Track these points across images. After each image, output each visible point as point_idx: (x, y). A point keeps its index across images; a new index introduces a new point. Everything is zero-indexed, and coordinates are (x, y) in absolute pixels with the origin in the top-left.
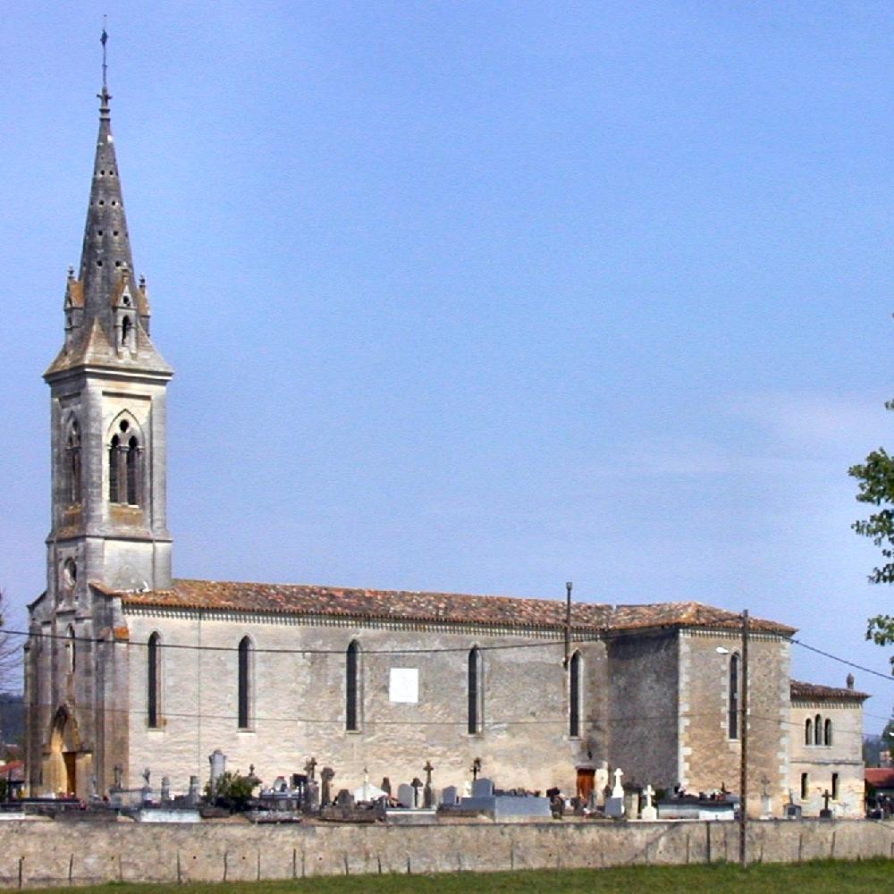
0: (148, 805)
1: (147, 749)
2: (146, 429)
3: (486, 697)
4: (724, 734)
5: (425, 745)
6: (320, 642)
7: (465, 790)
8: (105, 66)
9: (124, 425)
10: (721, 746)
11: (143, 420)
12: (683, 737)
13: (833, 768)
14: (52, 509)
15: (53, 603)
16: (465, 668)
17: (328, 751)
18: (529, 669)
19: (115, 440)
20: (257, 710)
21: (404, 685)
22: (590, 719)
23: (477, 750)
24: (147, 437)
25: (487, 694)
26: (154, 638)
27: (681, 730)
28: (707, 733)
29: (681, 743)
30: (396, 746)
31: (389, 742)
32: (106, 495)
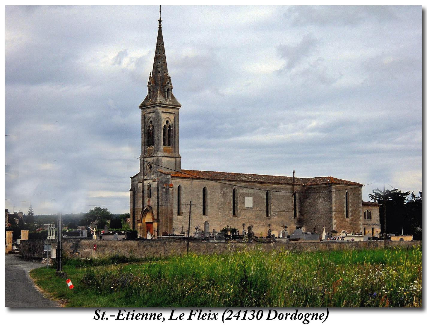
0: (212, 238)
1: (177, 221)
2: (173, 123)
3: (271, 205)
4: (345, 216)
5: (255, 220)
6: (225, 189)
7: (265, 235)
8: (160, 11)
9: (167, 122)
10: (344, 220)
11: (173, 121)
12: (334, 217)
13: (372, 226)
14: (142, 148)
15: (142, 177)
16: (265, 197)
17: (228, 222)
18: (283, 197)
19: (165, 126)
20: (209, 210)
21: (249, 202)
22: (299, 212)
23: (269, 222)
24: (174, 125)
25: (272, 205)
26: (179, 187)
27: (333, 215)
28: (340, 216)
29: (333, 219)
30: (247, 220)
31: (245, 219)
32: (162, 144)
